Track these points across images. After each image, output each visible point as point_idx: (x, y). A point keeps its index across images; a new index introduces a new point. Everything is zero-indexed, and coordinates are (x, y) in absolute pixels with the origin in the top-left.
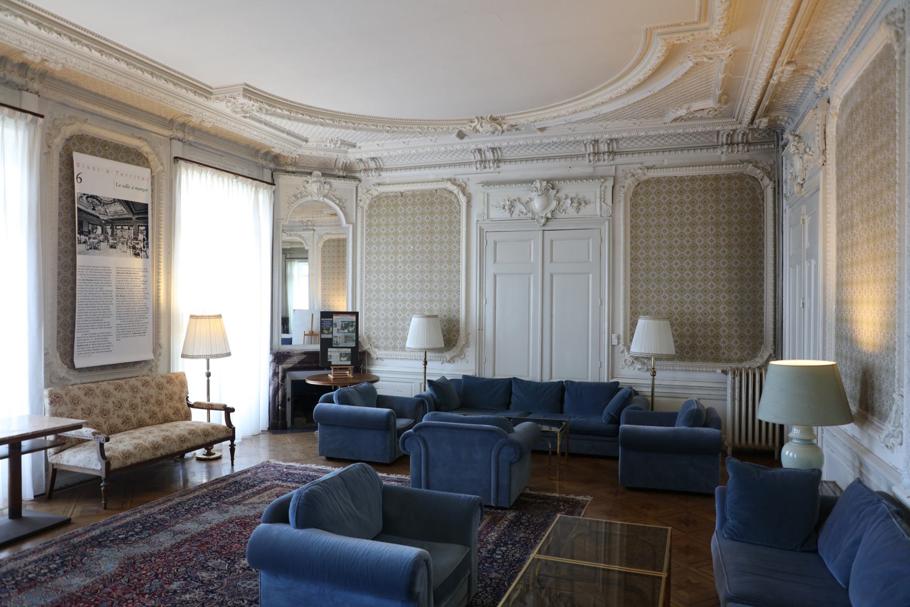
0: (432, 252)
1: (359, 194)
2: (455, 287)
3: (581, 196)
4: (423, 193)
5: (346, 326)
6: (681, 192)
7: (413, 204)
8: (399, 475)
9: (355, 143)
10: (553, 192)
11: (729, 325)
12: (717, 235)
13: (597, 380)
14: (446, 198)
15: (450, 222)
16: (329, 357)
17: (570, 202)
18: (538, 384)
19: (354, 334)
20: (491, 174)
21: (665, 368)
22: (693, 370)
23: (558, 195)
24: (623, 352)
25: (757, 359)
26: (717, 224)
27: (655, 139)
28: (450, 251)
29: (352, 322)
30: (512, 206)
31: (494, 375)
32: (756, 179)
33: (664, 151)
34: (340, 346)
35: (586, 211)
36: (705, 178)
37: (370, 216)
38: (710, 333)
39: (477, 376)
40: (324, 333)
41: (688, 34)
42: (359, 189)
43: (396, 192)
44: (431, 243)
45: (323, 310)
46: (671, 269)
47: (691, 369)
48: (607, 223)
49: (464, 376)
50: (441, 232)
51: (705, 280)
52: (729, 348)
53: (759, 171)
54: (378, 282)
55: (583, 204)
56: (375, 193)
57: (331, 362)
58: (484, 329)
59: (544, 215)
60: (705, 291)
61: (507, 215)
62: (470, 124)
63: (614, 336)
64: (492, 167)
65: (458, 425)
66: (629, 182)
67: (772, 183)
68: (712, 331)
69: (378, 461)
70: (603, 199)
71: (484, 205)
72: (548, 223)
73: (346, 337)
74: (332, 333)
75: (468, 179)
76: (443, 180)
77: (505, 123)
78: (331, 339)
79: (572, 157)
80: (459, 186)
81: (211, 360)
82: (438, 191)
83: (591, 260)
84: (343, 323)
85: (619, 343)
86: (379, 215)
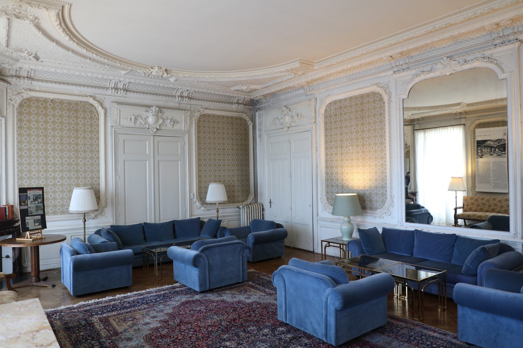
0: (77, 144)
1: (8, 95)
2: (95, 168)
3: (174, 118)
4: (69, 103)
5: (36, 198)
6: (218, 122)
7: (61, 109)
10: (160, 114)
11: (238, 186)
16: (27, 224)
17: (170, 121)
18: (154, 224)
19: (42, 204)
20: (120, 97)
23: (163, 116)
24: (195, 202)
25: (248, 200)
26: (233, 139)
27: (57, 75)
28: (91, 145)
29: (40, 195)
32: (246, 121)
33: (212, 101)
35: (177, 127)
36: (228, 117)
37: (20, 113)
39: (115, 225)
40: (22, 205)
41: (307, 65)
42: (9, 90)
43: (46, 98)
45: (21, 187)
48: (187, 135)
55: (176, 123)
56: (26, 96)
57: (28, 228)
58: (118, 195)
59: (155, 127)
60: (229, 170)
61: (132, 124)
63: (192, 194)
64: (121, 93)
66: (197, 115)
67: (252, 124)
68: (232, 189)
69: (124, 286)
71: (117, 116)
73: (37, 207)
74: (27, 205)
76: (86, 96)
77: (170, 74)
78: (27, 210)
79: (169, 96)
80: (99, 102)
82: (82, 103)
84: (34, 196)
85: (194, 198)
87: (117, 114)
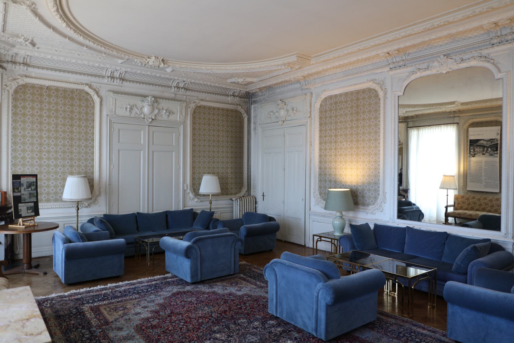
4: (65, 90)
5: (29, 185)
9: (36, 44)
10: (156, 104)
12: (227, 137)
13: (177, 210)
16: (20, 211)
17: (165, 112)
19: (35, 192)
22: (43, 208)
23: (158, 107)
24: (189, 193)
25: (241, 193)
26: (227, 131)
29: (34, 182)
31: (118, 212)
33: (208, 93)
34: (26, 201)
35: (172, 117)
36: (223, 109)
37: (15, 99)
38: (224, 182)
39: (108, 214)
42: (4, 76)
44: (72, 126)
48: (182, 126)
49: (104, 215)
50: (80, 119)
52: (231, 188)
54: (24, 151)
55: (171, 114)
60: (223, 162)
61: (127, 113)
63: (185, 185)
64: (117, 82)
66: (193, 106)
70: (181, 113)
71: (113, 105)
72: (153, 122)
73: (30, 194)
74: (20, 191)
75: (100, 87)
76: (82, 84)
77: (167, 64)
80: (95, 90)
81: (448, 190)
82: (78, 91)
83: (174, 144)
84: (28, 183)
85: (187, 189)
86: (24, 100)
87: (113, 103)
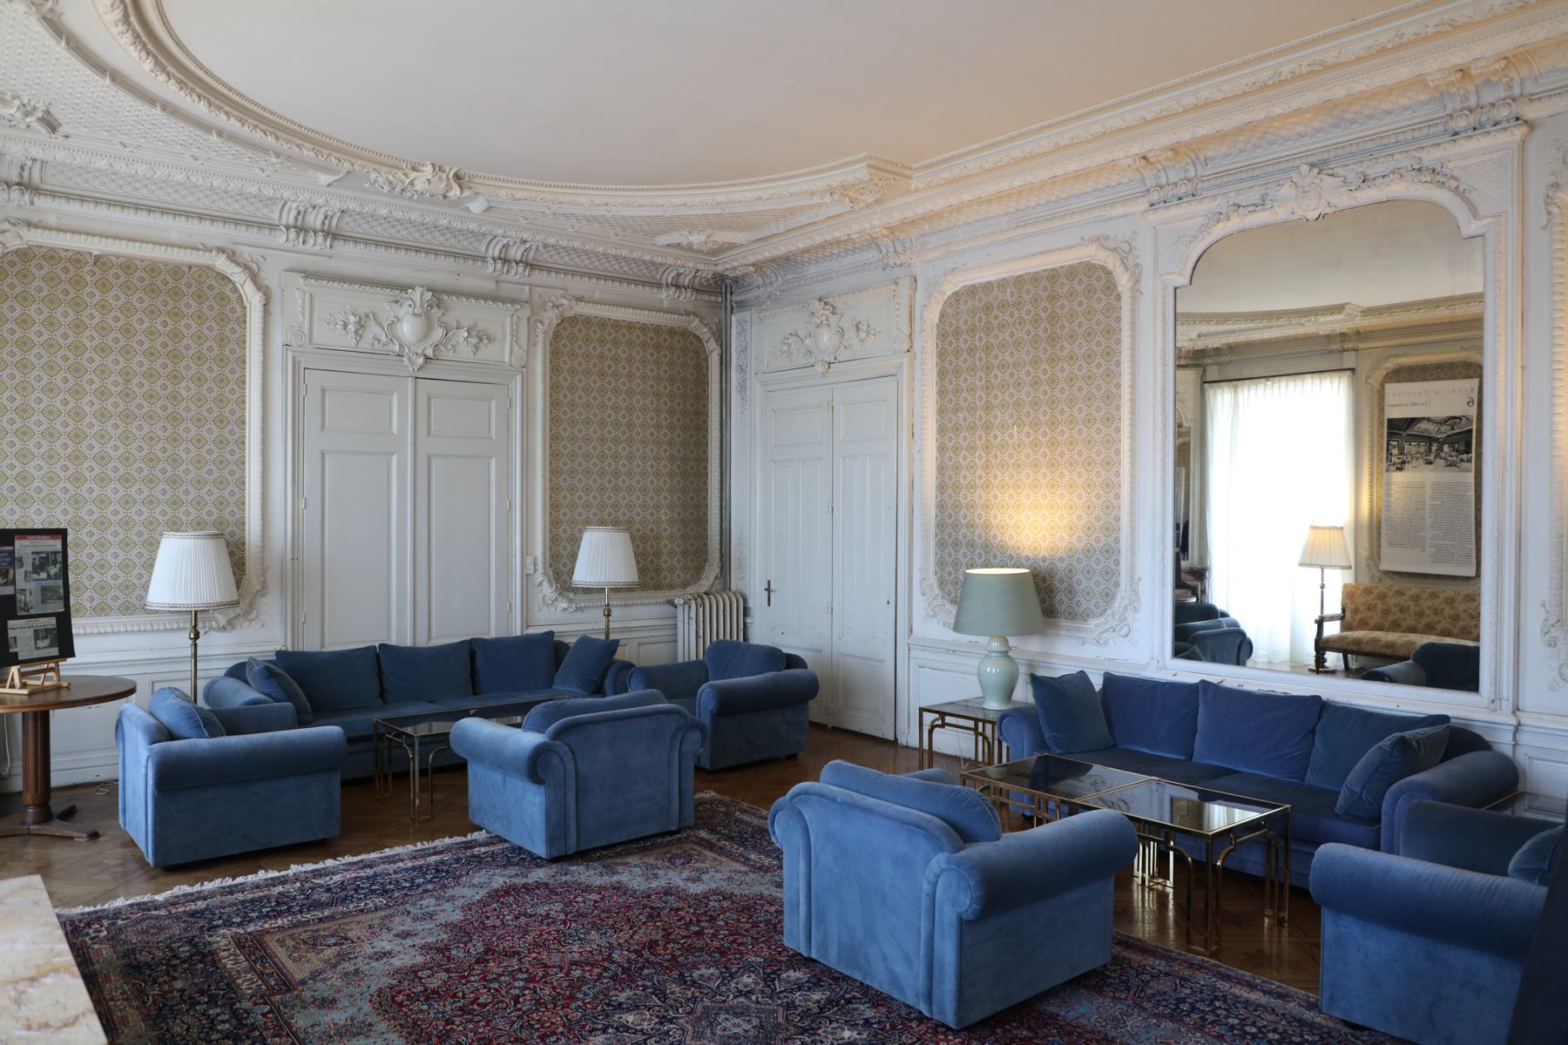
4: (153, 268)
5: (42, 563)
8: (219, 880)
10: (437, 313)
11: (671, 538)
13: (503, 634)
14: (211, 287)
15: (221, 341)
16: (11, 642)
19: (60, 582)
20: (313, 257)
21: (142, 629)
23: (445, 319)
26: (658, 395)
28: (220, 400)
29: (55, 553)
30: (361, 325)
33: (598, 277)
34: (32, 612)
35: (488, 352)
36: (644, 328)
39: (290, 650)
41: (891, 176)
46: (602, 456)
47: (631, 602)
48: (519, 378)
51: (644, 474)
52: (671, 569)
53: (705, 330)
55: (485, 341)
57: (16, 653)
59: (420, 352)
61: (349, 340)
62: (409, 171)
64: (317, 243)
65: (624, 713)
66: (551, 317)
68: (652, 546)
71: (303, 315)
72: (428, 366)
73: (44, 589)
74: (14, 582)
76: (208, 249)
77: (470, 188)
78: (12, 598)
80: (246, 267)
82: (193, 270)
84: (37, 557)
85: (535, 571)
